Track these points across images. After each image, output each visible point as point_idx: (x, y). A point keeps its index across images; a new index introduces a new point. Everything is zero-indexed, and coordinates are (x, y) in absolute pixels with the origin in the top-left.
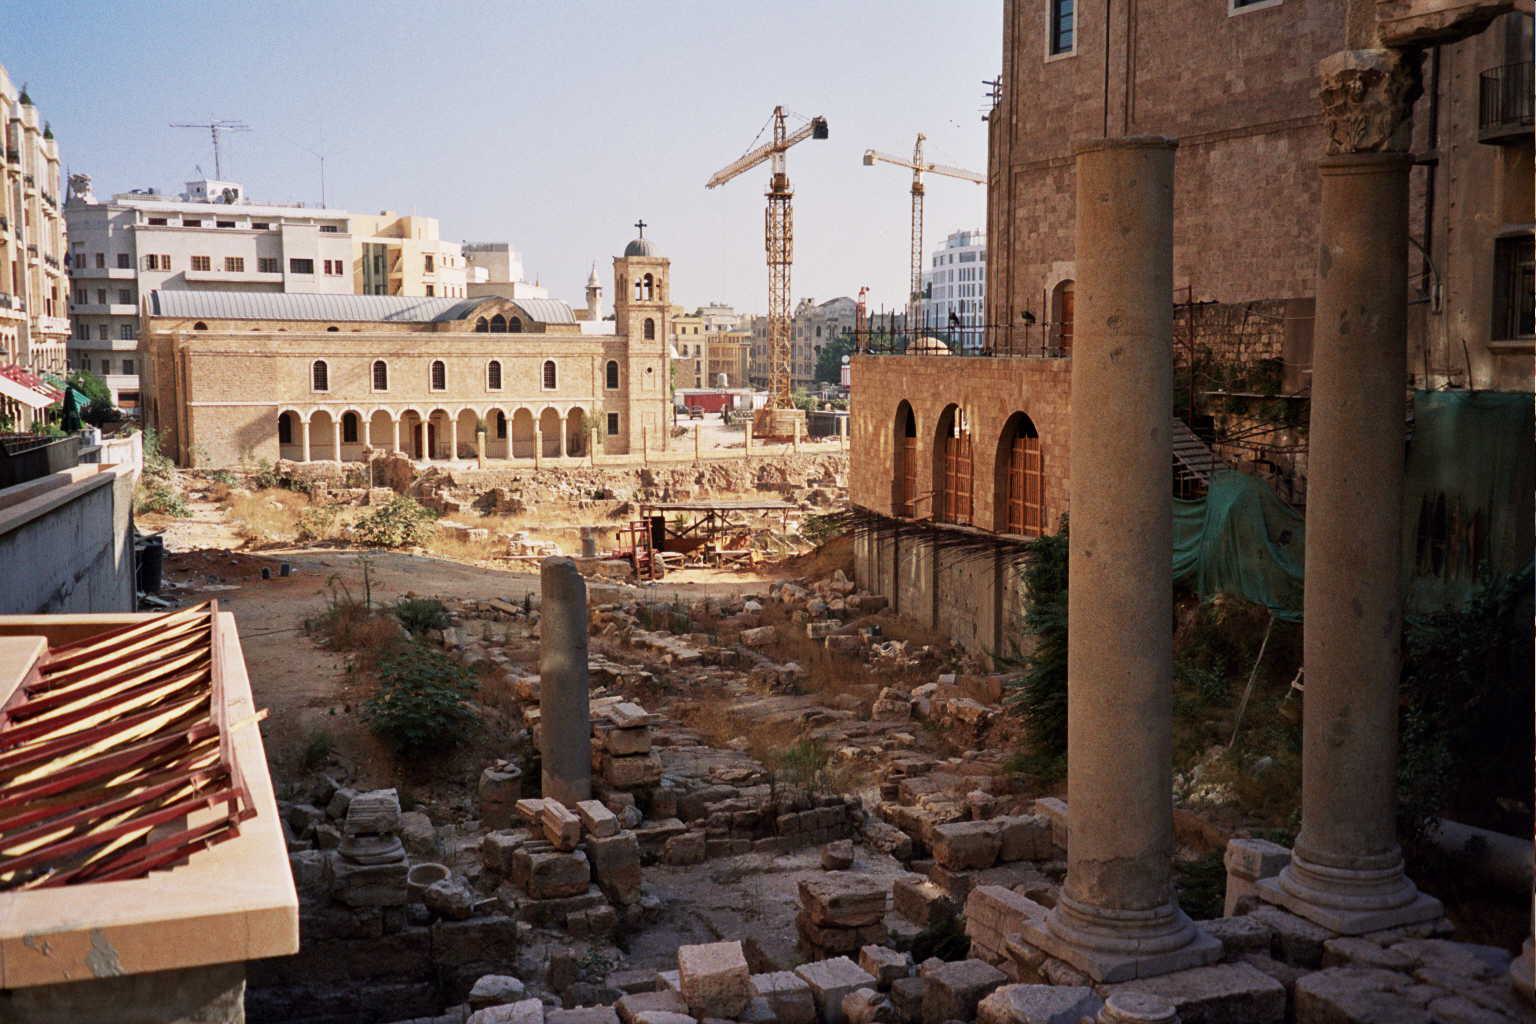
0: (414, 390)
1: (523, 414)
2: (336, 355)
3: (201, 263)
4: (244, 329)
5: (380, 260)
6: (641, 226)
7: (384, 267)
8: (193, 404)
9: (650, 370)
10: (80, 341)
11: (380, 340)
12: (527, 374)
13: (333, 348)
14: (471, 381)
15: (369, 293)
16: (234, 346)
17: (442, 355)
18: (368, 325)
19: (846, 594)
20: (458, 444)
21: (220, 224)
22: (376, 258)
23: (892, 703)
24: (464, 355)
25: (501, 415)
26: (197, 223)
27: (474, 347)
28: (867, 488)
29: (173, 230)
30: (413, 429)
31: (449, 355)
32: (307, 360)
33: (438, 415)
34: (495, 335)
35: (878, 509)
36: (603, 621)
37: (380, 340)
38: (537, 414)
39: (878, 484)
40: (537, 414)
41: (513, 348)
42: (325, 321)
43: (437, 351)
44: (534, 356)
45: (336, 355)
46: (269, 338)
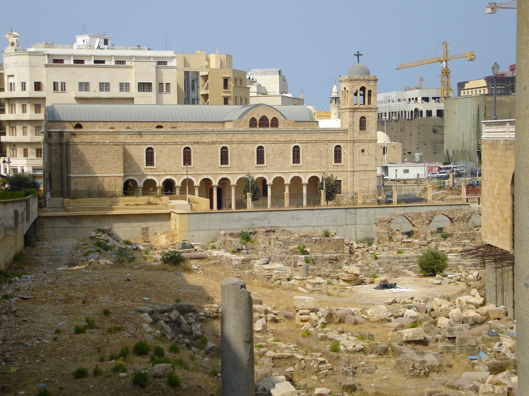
0: (208, 166)
1: (279, 181)
2: (160, 144)
3: (104, 86)
4: (104, 127)
5: (196, 82)
6: (358, 55)
7: (198, 87)
8: (72, 176)
9: (363, 151)
10: (11, 137)
11: (188, 133)
12: (281, 154)
13: (159, 139)
14: (245, 160)
15: (188, 104)
16: (97, 138)
17: (226, 142)
18: (182, 124)
19: (477, 306)
20: (236, 201)
21: (95, 62)
22: (193, 81)
23: (493, 388)
24: (241, 142)
25: (264, 181)
26: (82, 62)
27: (248, 137)
28: (493, 231)
29: (67, 66)
30: (208, 191)
31: (231, 142)
32: (142, 147)
33: (224, 182)
34: (261, 129)
35: (500, 246)
36: (302, 321)
37: (188, 133)
38: (287, 181)
39: (500, 228)
40: (287, 181)
41: (273, 138)
42: (154, 122)
43: (224, 140)
44: (286, 142)
45: (160, 144)
46: (119, 133)
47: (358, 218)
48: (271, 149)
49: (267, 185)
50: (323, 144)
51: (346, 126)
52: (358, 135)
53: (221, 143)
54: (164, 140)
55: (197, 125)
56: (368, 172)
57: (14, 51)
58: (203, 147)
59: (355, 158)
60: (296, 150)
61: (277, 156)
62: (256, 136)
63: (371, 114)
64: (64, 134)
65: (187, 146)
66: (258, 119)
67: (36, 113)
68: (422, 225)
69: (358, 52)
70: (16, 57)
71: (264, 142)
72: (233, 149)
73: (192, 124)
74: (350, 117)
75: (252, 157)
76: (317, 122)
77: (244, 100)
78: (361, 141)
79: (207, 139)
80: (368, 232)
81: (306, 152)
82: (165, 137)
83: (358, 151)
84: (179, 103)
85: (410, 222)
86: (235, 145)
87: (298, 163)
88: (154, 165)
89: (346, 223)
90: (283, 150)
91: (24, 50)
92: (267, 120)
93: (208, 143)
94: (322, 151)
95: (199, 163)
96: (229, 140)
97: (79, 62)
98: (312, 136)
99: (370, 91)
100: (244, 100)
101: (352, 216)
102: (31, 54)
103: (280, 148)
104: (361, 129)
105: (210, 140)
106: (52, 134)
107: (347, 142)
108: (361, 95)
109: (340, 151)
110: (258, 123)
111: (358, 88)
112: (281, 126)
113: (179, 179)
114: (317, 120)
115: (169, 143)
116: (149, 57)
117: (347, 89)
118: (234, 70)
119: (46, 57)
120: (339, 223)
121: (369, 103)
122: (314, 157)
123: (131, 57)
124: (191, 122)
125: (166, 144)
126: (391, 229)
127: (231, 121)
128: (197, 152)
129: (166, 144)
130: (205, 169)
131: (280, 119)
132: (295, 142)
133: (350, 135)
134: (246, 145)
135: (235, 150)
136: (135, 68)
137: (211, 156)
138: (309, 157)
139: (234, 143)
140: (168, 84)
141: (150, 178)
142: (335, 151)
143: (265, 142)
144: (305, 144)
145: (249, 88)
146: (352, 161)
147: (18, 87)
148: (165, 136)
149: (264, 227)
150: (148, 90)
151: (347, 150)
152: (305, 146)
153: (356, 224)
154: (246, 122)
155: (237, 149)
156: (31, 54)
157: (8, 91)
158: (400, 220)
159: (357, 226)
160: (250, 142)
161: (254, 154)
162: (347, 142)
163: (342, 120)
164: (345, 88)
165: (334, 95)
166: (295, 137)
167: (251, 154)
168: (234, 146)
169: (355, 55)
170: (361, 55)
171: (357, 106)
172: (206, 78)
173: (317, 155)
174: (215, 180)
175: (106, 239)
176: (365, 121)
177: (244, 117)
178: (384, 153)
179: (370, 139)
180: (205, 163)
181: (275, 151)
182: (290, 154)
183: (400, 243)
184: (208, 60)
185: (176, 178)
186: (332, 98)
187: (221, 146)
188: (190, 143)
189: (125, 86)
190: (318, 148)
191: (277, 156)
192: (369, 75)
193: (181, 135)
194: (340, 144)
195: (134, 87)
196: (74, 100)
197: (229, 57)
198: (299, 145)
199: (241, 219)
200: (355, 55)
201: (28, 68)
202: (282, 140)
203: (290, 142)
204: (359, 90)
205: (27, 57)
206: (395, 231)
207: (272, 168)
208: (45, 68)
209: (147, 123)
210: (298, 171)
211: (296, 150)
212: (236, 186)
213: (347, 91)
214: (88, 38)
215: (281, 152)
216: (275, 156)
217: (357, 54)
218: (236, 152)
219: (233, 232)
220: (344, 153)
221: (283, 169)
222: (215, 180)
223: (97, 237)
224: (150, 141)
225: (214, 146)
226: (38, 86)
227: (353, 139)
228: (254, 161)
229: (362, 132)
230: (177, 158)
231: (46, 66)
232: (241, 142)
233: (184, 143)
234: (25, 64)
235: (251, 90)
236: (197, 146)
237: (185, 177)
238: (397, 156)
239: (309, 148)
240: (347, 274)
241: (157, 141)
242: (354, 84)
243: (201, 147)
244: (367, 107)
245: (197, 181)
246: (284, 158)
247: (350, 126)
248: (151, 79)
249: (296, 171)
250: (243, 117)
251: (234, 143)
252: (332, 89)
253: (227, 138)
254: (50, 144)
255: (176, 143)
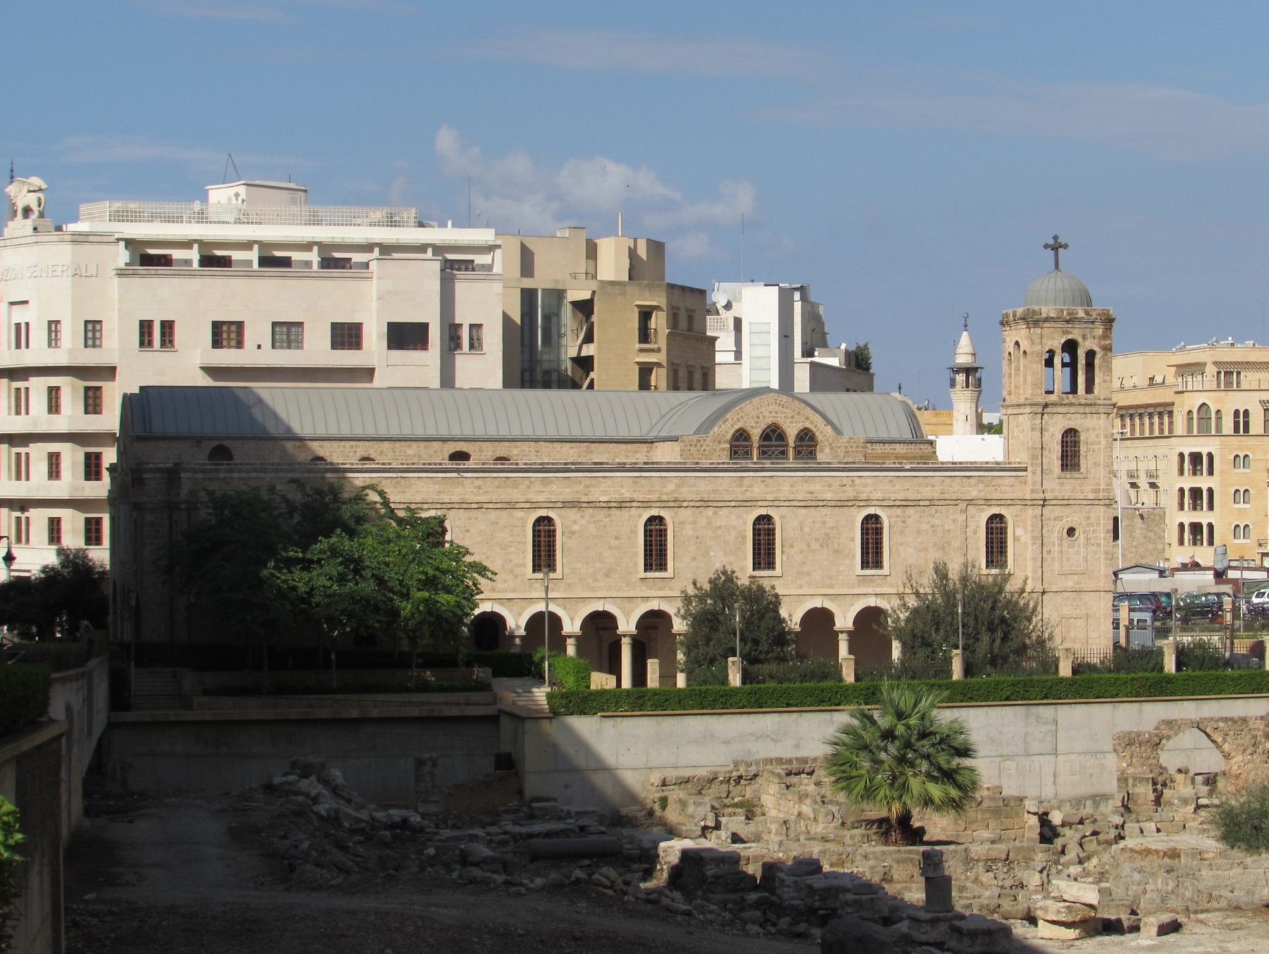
2: (464, 506)
3: (286, 333)
6: (1056, 247)
9: (1071, 531)
24: (704, 504)
27: (727, 484)
31: (678, 504)
42: (445, 440)
43: (654, 497)
44: (841, 504)
47: (1061, 734)
48: (796, 524)
49: (836, 634)
50: (951, 509)
51: (1021, 458)
52: (1057, 484)
53: (646, 504)
54: (477, 495)
55: (572, 451)
56: (1085, 596)
57: (30, 231)
58: (592, 516)
59: (1049, 552)
60: (872, 528)
61: (815, 546)
62: (751, 486)
63: (1095, 421)
64: (182, 475)
65: (543, 513)
66: (756, 434)
67: (86, 412)
68: (1252, 754)
69: (1055, 238)
70: (36, 248)
71: (775, 503)
72: (682, 523)
73: (558, 445)
74: (1033, 429)
75: (739, 548)
76: (931, 443)
77: (698, 376)
78: (1066, 503)
79: (605, 493)
80: (1091, 775)
81: (902, 532)
82: (479, 488)
83: (1055, 532)
84: (507, 383)
85: (1218, 746)
86: (689, 512)
87: (769, 568)
88: (881, 567)
89: (1026, 750)
90: (832, 528)
91: (59, 229)
92: (781, 437)
93: (608, 506)
94: (949, 531)
95: (579, 565)
96: (671, 498)
97: (213, 260)
98: (919, 485)
99: (1091, 355)
100: (698, 376)
101: (1044, 728)
102: (80, 239)
103: (824, 523)
104: (1064, 467)
105: (615, 497)
106: (145, 476)
107: (1024, 503)
108: (1064, 365)
109: (1003, 531)
110: (756, 445)
111: (1056, 342)
112: (823, 456)
113: (520, 614)
114: (931, 438)
115: (490, 506)
116: (422, 248)
117: (1024, 345)
118: (671, 287)
119: (122, 244)
120: (1006, 751)
121: (1089, 388)
122: (925, 549)
123: (368, 247)
124: (552, 441)
125: (480, 506)
126: (1161, 768)
127: (675, 439)
128: (573, 533)
129: (480, 506)
130: (597, 584)
131: (823, 432)
132: (868, 502)
133: (1034, 483)
134: (723, 512)
135: (687, 526)
136: (379, 278)
137: (614, 543)
138: (911, 550)
139: (685, 504)
140: (475, 327)
141: (489, 610)
142: (989, 531)
143: (777, 503)
144: (899, 511)
145: (715, 339)
146: (1040, 563)
147: (39, 335)
148: (478, 483)
149: (780, 761)
150: (285, 345)
151: (1025, 529)
152: (898, 516)
153: (1056, 754)
154: (720, 442)
155: (694, 523)
156: (80, 239)
157: (9, 348)
158: (1191, 738)
159: (1060, 758)
160: (733, 504)
161: (744, 537)
162: (1024, 503)
163: (1007, 439)
164: (1017, 343)
165: (963, 359)
166: (869, 488)
167: (737, 538)
168: (685, 514)
169: (1046, 246)
170: (1066, 246)
171: (1053, 398)
172: (585, 308)
173: (935, 544)
174: (627, 615)
175: (313, 793)
176: (1076, 443)
177: (716, 429)
178: (1116, 537)
179: (1091, 496)
180: (598, 565)
181: (807, 529)
182: (853, 540)
183: (1191, 808)
184: (592, 251)
185: (511, 611)
186: (959, 370)
187: (647, 515)
188: (552, 505)
189: (347, 335)
190: (937, 522)
191: (815, 546)
192: (1089, 303)
193: (527, 482)
194: (1003, 511)
195: (374, 336)
196: (201, 373)
197: (657, 248)
198: (879, 512)
199: (712, 736)
200: (1046, 246)
201: (70, 279)
202: (829, 496)
203: (853, 502)
204: (1058, 351)
205: (68, 248)
206: (1172, 771)
207: (799, 582)
208: (117, 279)
209: (422, 444)
210: (878, 590)
211: (872, 528)
212: (577, 638)
213: (1025, 352)
214: (242, 190)
215: (827, 535)
216: (809, 546)
217: (1051, 242)
218: (690, 533)
219: (687, 773)
220: (1016, 539)
221: (831, 586)
222: (627, 615)
223: (286, 787)
224: (435, 498)
225: (625, 513)
226: (92, 332)
227: (1041, 496)
228: (745, 558)
229: (1068, 474)
230: (512, 549)
231: (121, 273)
232: (704, 504)
233: (535, 506)
234: (59, 269)
235: (718, 345)
236: (572, 514)
237: (540, 607)
238: (1151, 547)
239: (909, 521)
240: (1062, 904)
241: (456, 498)
242: (1046, 331)
243: (587, 517)
244: (1083, 401)
245: (572, 619)
246: (836, 551)
247: (1034, 457)
248: (430, 315)
249: (870, 590)
250: (711, 427)
251: (685, 504)
252: (955, 343)
253: (665, 490)
254: (138, 507)
255: (511, 506)
